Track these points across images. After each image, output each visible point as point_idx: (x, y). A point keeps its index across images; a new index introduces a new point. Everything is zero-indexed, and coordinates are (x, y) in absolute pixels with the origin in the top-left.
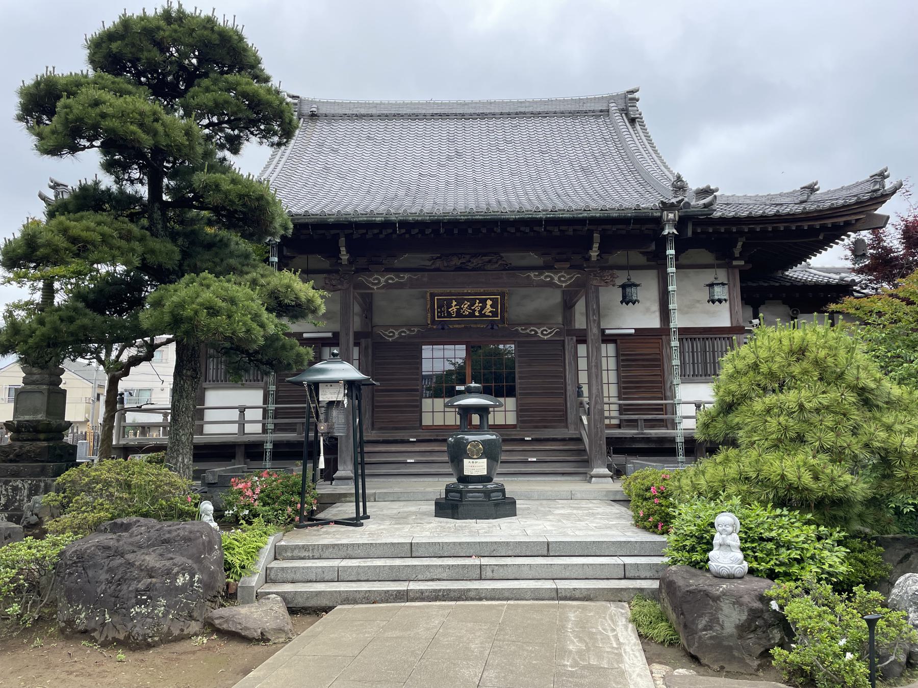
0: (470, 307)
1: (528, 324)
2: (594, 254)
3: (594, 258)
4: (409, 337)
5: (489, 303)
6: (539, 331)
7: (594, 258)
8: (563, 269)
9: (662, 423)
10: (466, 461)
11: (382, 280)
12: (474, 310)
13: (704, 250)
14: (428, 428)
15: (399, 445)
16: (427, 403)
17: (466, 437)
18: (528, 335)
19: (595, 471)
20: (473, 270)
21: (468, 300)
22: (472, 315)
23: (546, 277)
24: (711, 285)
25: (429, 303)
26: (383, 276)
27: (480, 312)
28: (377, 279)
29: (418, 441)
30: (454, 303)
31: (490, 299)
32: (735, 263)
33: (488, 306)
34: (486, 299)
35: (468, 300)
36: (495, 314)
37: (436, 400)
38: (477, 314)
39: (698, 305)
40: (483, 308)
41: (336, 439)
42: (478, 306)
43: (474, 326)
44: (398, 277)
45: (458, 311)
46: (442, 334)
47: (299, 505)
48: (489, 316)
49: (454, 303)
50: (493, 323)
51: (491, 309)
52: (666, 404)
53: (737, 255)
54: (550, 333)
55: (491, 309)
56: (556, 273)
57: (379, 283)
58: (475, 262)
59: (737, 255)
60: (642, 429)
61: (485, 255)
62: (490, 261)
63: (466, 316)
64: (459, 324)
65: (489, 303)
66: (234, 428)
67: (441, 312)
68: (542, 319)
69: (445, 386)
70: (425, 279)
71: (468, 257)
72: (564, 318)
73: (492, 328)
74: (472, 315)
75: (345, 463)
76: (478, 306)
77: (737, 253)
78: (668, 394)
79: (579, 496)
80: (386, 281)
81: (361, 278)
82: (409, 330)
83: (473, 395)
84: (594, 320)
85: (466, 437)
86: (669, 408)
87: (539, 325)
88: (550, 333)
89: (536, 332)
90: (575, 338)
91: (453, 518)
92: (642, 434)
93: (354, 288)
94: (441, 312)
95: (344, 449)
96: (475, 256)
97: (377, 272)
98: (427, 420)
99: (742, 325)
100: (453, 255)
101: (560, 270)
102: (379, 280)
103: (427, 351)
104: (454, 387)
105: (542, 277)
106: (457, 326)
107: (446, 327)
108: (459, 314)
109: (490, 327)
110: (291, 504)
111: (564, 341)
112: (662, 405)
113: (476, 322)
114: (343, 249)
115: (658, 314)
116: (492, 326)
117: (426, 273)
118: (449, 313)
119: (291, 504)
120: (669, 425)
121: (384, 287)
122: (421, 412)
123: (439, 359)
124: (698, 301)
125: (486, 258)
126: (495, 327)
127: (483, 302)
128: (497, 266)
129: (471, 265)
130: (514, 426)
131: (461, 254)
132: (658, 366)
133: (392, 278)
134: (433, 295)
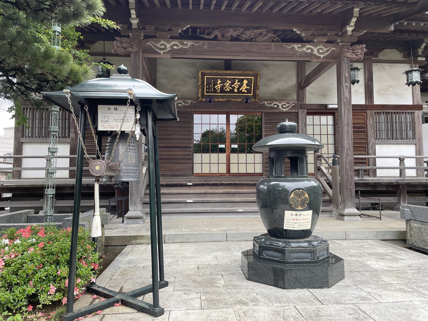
0: (231, 84)
1: (272, 100)
2: (350, 29)
3: (349, 33)
4: (184, 107)
5: (245, 82)
6: (280, 105)
7: (349, 33)
8: (321, 42)
9: (367, 172)
10: (288, 214)
11: (168, 46)
12: (234, 88)
13: (395, 50)
14: (198, 175)
15: (179, 188)
16: (197, 157)
17: (282, 184)
18: (272, 108)
19: (347, 211)
20: (246, 40)
21: (229, 79)
22: (232, 91)
23: (308, 49)
24: (407, 73)
25: (200, 80)
26: (169, 43)
27: (238, 89)
28: (163, 44)
29: (194, 185)
30: (219, 81)
31: (246, 79)
32: (419, 59)
33: (244, 85)
34: (243, 80)
35: (229, 79)
36: (249, 91)
37: (204, 155)
38: (236, 90)
39: (391, 89)
40: (240, 86)
41: (127, 183)
42: (237, 84)
43: (234, 100)
44: (182, 44)
45: (222, 87)
46: (210, 106)
47: (67, 281)
48: (244, 93)
49: (219, 81)
50: (247, 98)
51: (246, 87)
52: (368, 158)
53: (420, 53)
54: (288, 107)
55: (246, 87)
56: (315, 46)
57: (165, 48)
58: (248, 34)
59: (420, 53)
60: (362, 177)
61: (257, 28)
62: (260, 34)
63: (227, 92)
64: (222, 98)
65: (245, 82)
66: (42, 174)
67: (209, 88)
68: (282, 96)
69: (212, 143)
70: (206, 47)
71: (241, 30)
72: (298, 96)
73: (247, 102)
74: (232, 91)
75: (135, 204)
76: (237, 84)
77: (420, 52)
78: (371, 151)
79: (352, 236)
80: (172, 47)
81: (150, 43)
82: (184, 102)
83: (287, 134)
84: (347, 87)
85: (282, 184)
86: (371, 162)
87: (280, 101)
88: (288, 107)
89: (278, 106)
90: (306, 111)
91: (276, 285)
92: (363, 180)
93: (143, 52)
94: (209, 88)
95: (135, 192)
96: (248, 28)
97: (164, 38)
98: (197, 169)
99: (421, 103)
100: (230, 27)
101: (320, 43)
102: (166, 46)
103: (197, 118)
104: (218, 145)
105: (304, 49)
106: (221, 100)
107: (212, 100)
108: (222, 90)
109: (245, 101)
110: (55, 279)
111: (298, 113)
112: (365, 159)
113: (235, 97)
114: (133, 12)
115: (363, 95)
116: (247, 99)
117: (207, 42)
118: (215, 89)
119: (55, 279)
120: (371, 174)
121: (169, 52)
122: (193, 163)
123: (205, 123)
124: (391, 87)
125: (257, 31)
126: (249, 101)
127: (241, 81)
128: (266, 38)
129: (244, 37)
130: (261, 174)
131: (237, 27)
132: (364, 132)
133: (177, 45)
134: (203, 75)
